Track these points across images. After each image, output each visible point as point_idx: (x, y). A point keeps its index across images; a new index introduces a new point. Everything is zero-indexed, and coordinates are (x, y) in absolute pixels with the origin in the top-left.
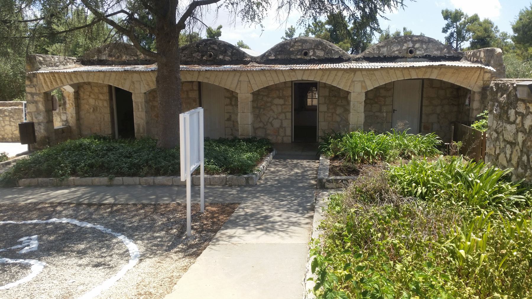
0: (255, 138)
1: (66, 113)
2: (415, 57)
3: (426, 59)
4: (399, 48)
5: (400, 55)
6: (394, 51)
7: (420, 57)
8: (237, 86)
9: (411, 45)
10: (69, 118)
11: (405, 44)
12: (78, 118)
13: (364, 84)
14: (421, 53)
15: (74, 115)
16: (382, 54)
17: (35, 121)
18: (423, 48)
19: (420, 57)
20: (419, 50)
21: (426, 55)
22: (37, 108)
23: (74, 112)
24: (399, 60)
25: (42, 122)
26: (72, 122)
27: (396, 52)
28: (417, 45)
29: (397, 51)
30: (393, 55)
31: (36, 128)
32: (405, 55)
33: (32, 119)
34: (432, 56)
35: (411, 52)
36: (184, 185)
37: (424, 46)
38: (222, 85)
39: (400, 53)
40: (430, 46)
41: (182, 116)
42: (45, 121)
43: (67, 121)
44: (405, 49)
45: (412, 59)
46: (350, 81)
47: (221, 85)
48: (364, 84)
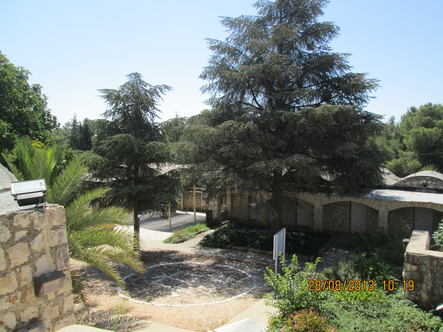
0: (256, 298)
1: (226, 204)
2: (428, 189)
3: (435, 191)
4: (417, 183)
5: (418, 187)
6: (414, 185)
7: (431, 189)
8: (314, 201)
9: (425, 182)
10: (228, 207)
11: (421, 181)
12: (232, 207)
13: (387, 207)
14: (432, 187)
15: (230, 205)
16: (406, 185)
17: (213, 210)
18: (433, 184)
19: (431, 189)
20: (431, 185)
21: (435, 189)
22: (214, 203)
23: (230, 203)
24: (417, 190)
25: (216, 211)
26: (229, 208)
27: (416, 185)
28: (429, 182)
29: (416, 184)
30: (413, 186)
31: (213, 213)
32: (421, 187)
33: (211, 209)
34: (439, 189)
35: (425, 186)
36: (275, 261)
37: (434, 183)
38: (306, 200)
39: (418, 186)
40: (438, 183)
41: (275, 236)
42: (218, 210)
43: (226, 208)
44: (421, 184)
45: (426, 190)
46: (379, 204)
47: (305, 200)
48: (387, 207)
